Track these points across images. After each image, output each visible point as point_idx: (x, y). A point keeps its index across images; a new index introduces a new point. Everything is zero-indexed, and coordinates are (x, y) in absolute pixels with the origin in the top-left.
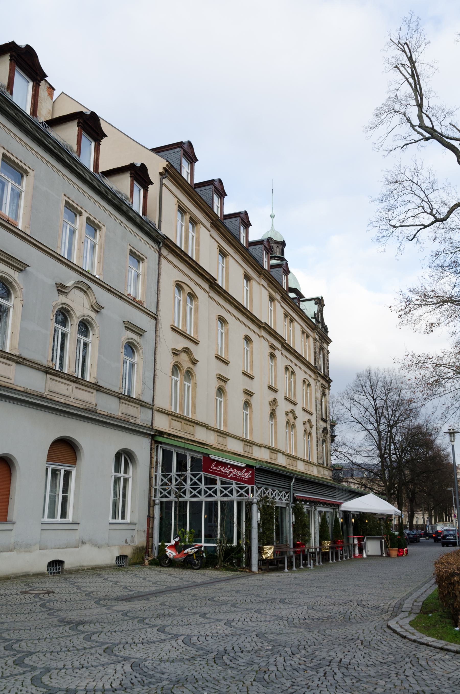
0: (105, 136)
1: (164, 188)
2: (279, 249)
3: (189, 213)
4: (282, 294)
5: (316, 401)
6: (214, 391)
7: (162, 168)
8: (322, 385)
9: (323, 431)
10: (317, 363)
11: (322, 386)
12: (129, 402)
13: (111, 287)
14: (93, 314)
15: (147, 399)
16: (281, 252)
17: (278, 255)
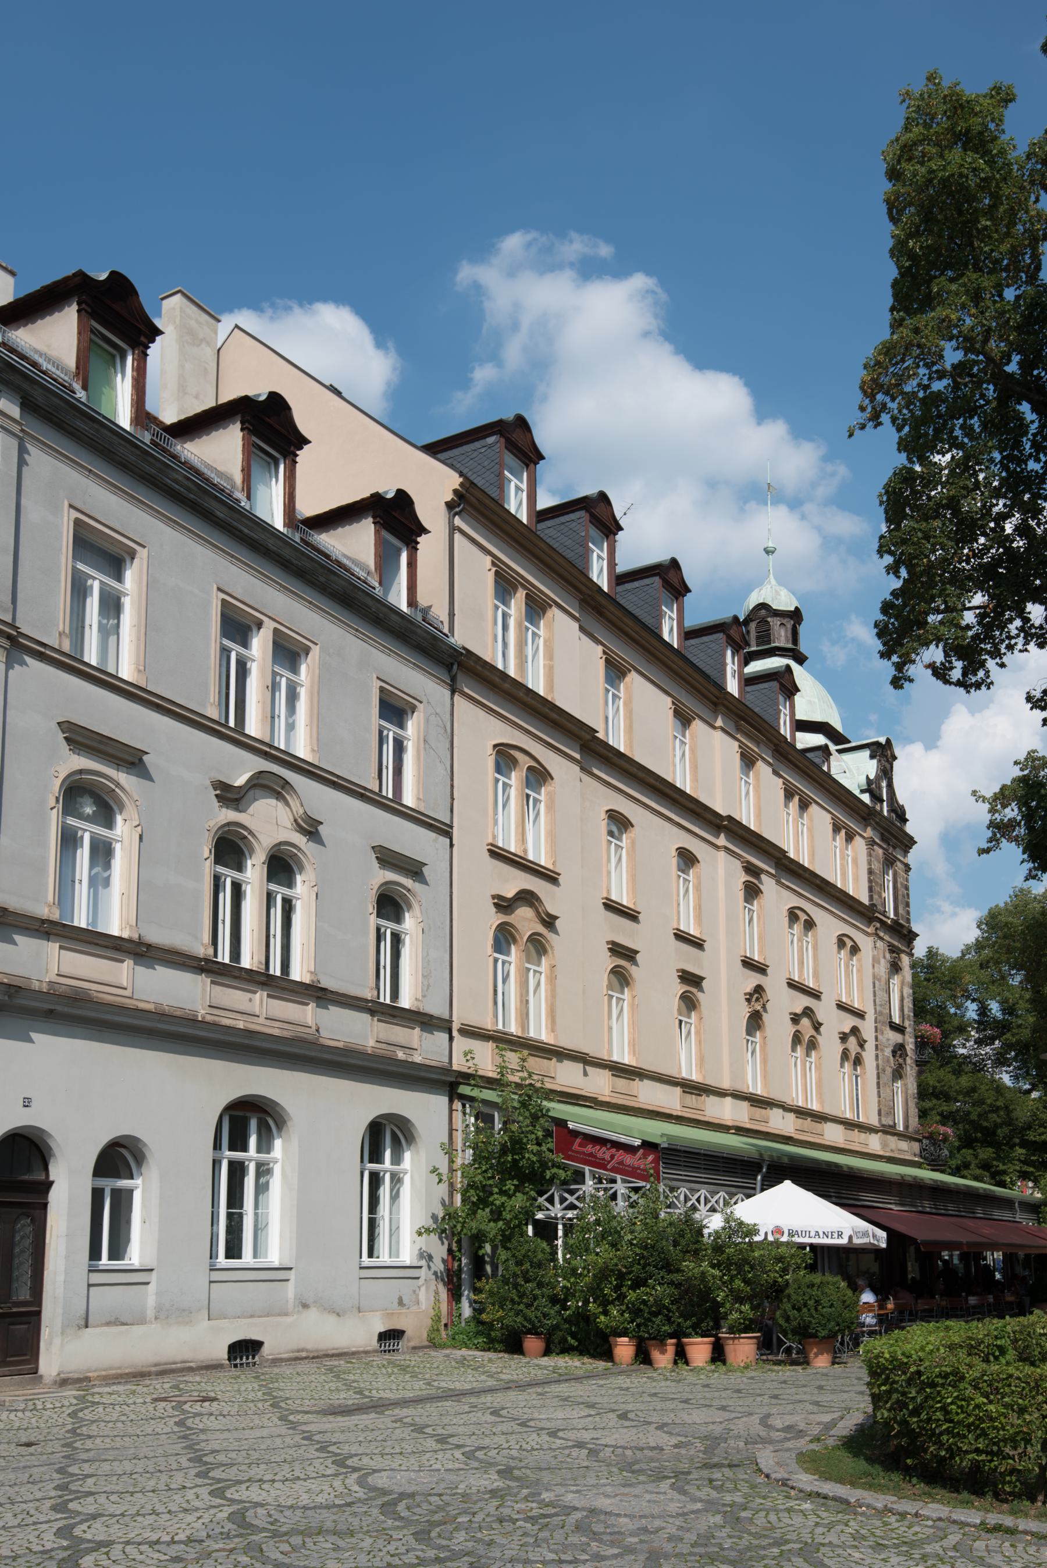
0: (307, 442)
1: (457, 536)
2: (786, 631)
3: (523, 586)
4: (775, 745)
5: (874, 983)
6: (604, 978)
7: (451, 492)
8: (890, 945)
9: (894, 1053)
10: (875, 897)
11: (893, 949)
12: (394, 1016)
13: (338, 777)
14: (300, 840)
15: (436, 1008)
16: (790, 635)
17: (782, 645)
